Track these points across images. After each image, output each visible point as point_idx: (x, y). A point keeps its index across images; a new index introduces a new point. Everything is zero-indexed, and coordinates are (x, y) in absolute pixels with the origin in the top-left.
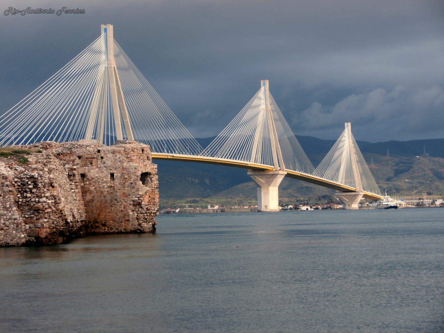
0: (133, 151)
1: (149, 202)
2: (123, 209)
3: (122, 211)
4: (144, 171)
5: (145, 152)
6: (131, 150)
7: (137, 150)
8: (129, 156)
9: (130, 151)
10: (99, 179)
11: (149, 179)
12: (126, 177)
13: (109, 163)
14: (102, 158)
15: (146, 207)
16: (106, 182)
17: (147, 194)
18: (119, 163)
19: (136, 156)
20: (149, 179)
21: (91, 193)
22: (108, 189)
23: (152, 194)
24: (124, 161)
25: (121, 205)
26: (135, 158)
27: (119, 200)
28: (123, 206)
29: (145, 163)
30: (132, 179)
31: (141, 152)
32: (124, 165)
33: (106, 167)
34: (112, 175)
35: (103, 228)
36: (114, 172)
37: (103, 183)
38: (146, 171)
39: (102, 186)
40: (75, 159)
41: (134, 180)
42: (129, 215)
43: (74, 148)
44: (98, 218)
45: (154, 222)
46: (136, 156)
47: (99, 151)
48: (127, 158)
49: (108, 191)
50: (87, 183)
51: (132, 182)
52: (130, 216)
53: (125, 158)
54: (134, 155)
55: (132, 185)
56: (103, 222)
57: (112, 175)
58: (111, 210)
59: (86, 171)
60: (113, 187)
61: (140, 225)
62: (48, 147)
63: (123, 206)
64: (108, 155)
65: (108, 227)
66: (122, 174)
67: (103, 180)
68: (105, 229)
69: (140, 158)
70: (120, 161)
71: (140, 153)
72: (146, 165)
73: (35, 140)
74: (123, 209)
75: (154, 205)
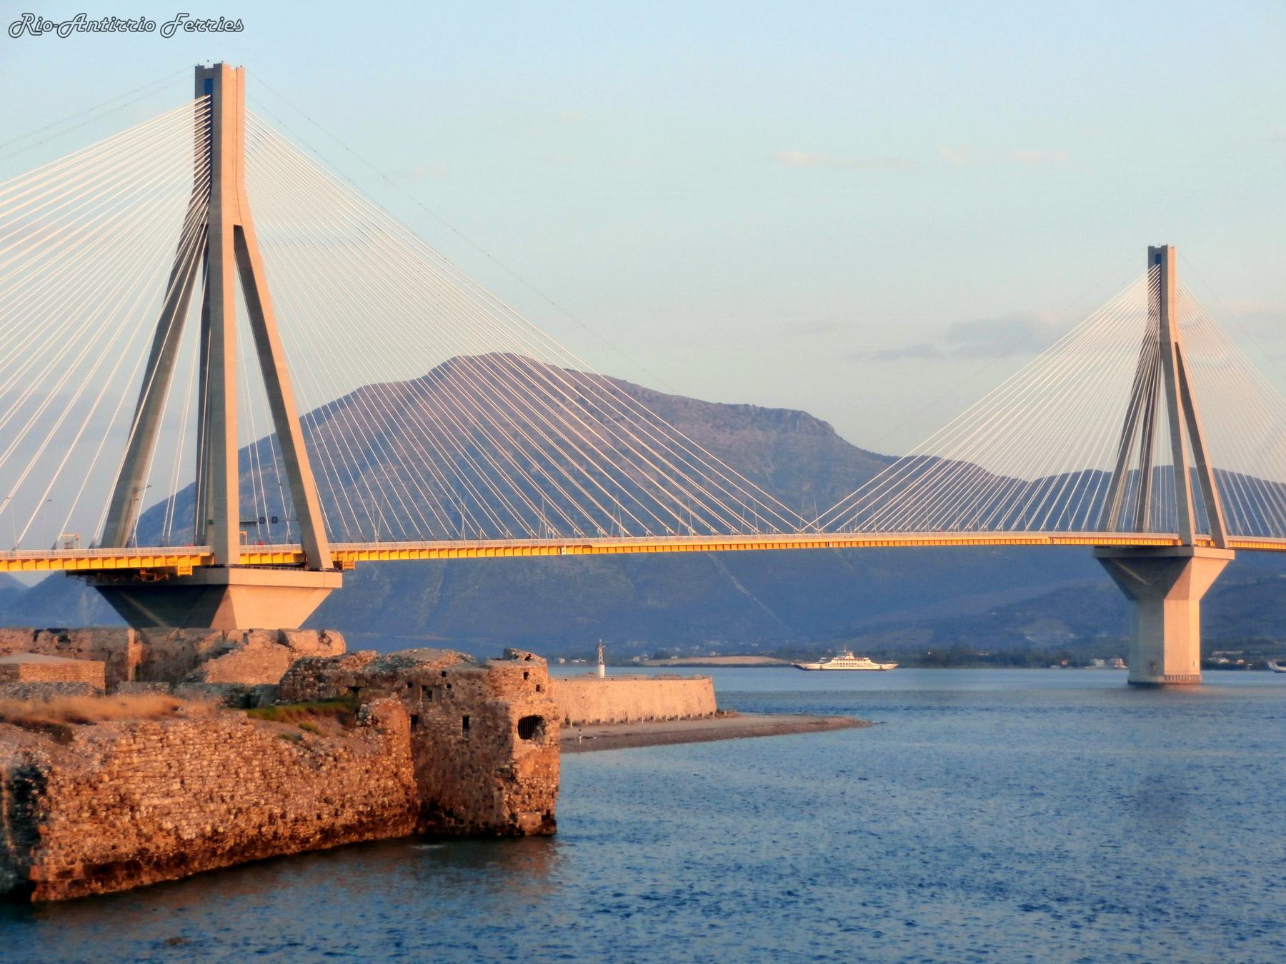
0: (505, 675)
1: (535, 772)
2: (482, 785)
3: (481, 788)
4: (527, 714)
5: (531, 677)
6: (501, 673)
7: (514, 673)
8: (497, 684)
9: (498, 675)
10: (442, 726)
11: (538, 728)
12: (489, 723)
13: (460, 696)
14: (449, 686)
15: (528, 782)
16: (455, 733)
17: (532, 757)
18: (478, 697)
19: (513, 684)
20: (538, 728)
21: (427, 752)
22: (458, 747)
23: (106, 826)
24: (488, 694)
25: (480, 777)
26: (509, 687)
27: (476, 768)
28: (482, 779)
29: (530, 699)
30: (501, 730)
31: (523, 678)
32: (487, 702)
33: (455, 704)
34: (466, 719)
35: (447, 819)
36: (469, 713)
37: (449, 734)
38: (532, 714)
39: (446, 739)
40: (402, 687)
41: (504, 731)
42: (493, 797)
43: (401, 666)
44: (438, 801)
45: (545, 811)
46: (513, 684)
47: (444, 674)
48: (494, 688)
49: (457, 750)
50: (422, 733)
51: (500, 734)
52: (495, 800)
53: (490, 689)
54: (507, 682)
55: (504, 741)
56: (448, 808)
57: (466, 719)
58: (462, 785)
59: (420, 711)
60: (467, 742)
61: (513, 816)
62: (358, 662)
63: (482, 779)
64: (458, 682)
65: (455, 818)
66: (484, 718)
67: (449, 728)
68: (450, 822)
69: (519, 688)
70: (480, 694)
71: (521, 680)
72: (532, 702)
73: (1028, 523)
74: (482, 785)
75: (547, 778)
